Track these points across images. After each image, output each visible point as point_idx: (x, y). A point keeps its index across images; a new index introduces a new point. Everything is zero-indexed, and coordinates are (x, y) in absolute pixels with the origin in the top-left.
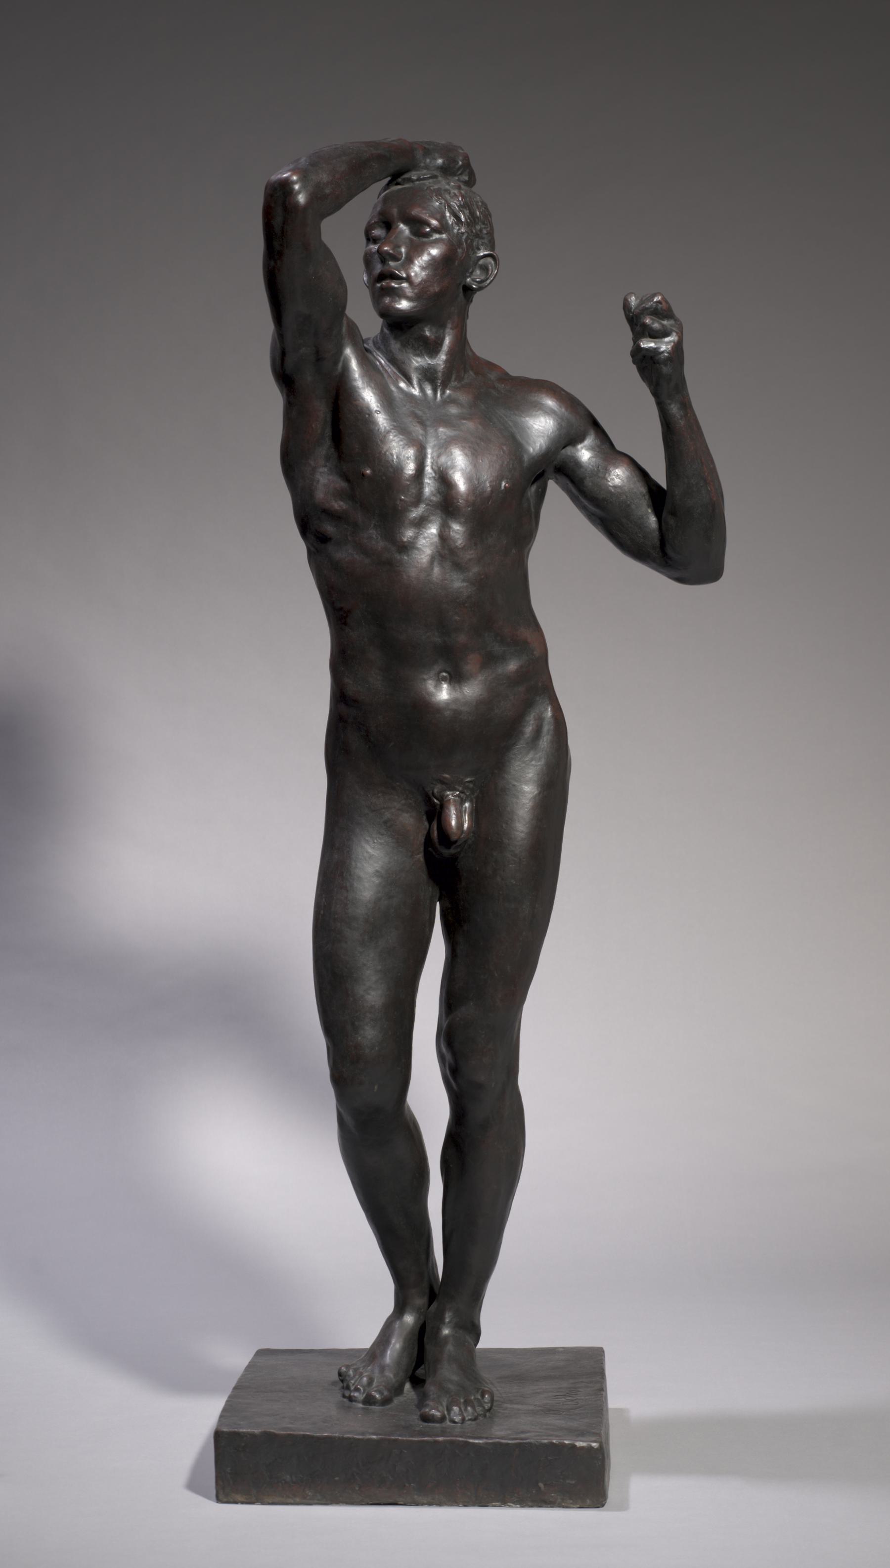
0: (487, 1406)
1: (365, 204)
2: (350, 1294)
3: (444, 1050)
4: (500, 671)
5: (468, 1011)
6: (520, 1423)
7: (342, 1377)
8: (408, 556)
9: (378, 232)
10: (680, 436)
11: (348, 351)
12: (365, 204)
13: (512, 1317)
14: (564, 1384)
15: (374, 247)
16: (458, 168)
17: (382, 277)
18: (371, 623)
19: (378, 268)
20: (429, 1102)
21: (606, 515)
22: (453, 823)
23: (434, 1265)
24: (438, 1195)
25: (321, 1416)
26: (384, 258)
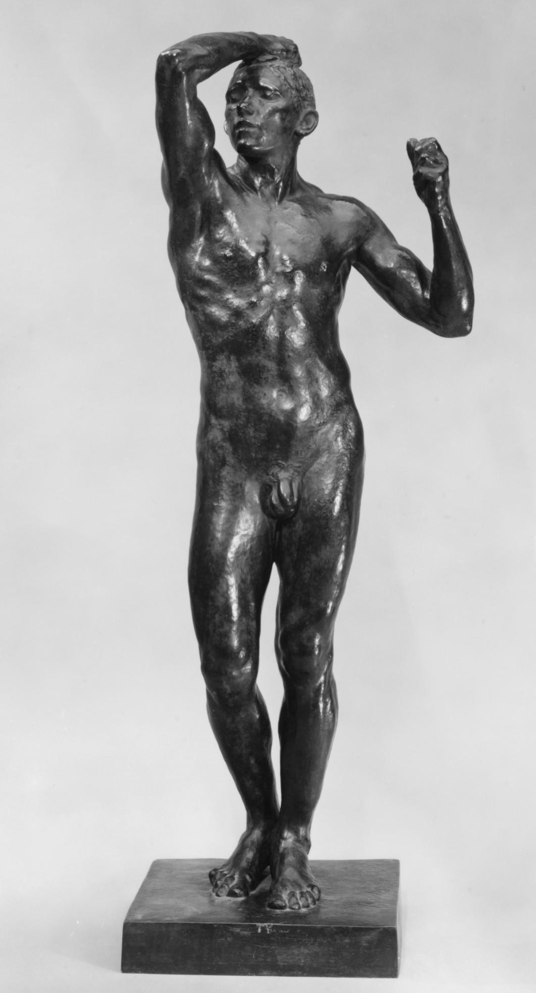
1: (226, 75)
2: (211, 822)
3: (279, 646)
4: (203, 135)
5: (294, 617)
6: (333, 906)
8: (317, 556)
9: (234, 96)
10: (446, 238)
11: (275, 567)
12: (226, 75)
15: (234, 106)
16: (291, 53)
17: (241, 124)
19: (237, 120)
20: (271, 687)
21: (386, 284)
22: (218, 194)
23: (275, 801)
24: (275, 753)
25: (193, 906)
26: (240, 112)
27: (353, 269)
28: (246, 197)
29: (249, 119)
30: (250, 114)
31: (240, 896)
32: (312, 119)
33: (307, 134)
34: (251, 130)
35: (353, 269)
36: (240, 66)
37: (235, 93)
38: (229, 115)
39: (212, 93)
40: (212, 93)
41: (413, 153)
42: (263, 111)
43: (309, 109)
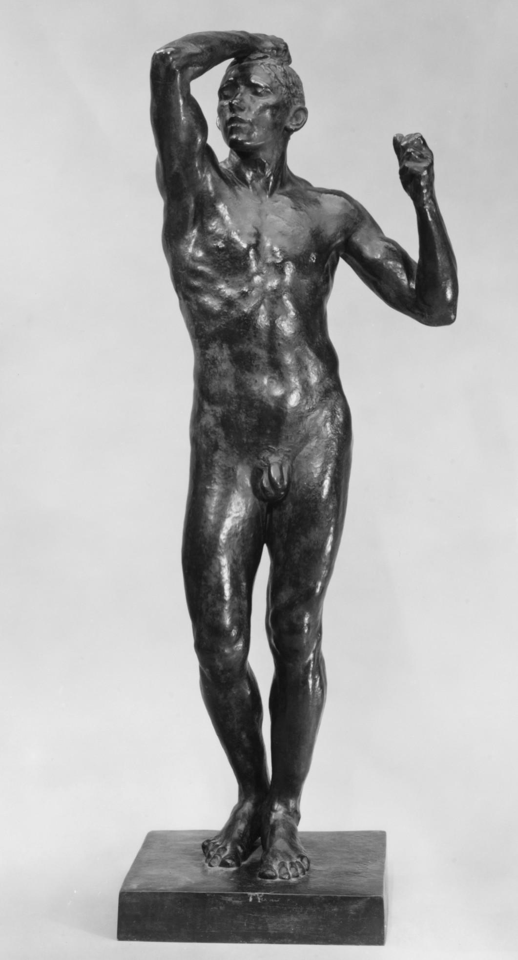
0: (305, 867)
1: (219, 72)
2: (204, 794)
3: (270, 624)
5: (285, 596)
7: (204, 847)
8: (307, 537)
9: (226, 93)
10: (431, 230)
12: (219, 72)
13: (322, 807)
14: (279, 183)
15: (226, 103)
16: (281, 51)
17: (233, 120)
18: (225, 341)
19: (229, 116)
23: (266, 775)
24: (266, 728)
25: (186, 876)
26: (232, 108)
27: (341, 260)
28: (238, 191)
29: (241, 115)
30: (242, 110)
31: (232, 866)
32: (302, 115)
33: (296, 130)
34: (243, 126)
35: (341, 260)
36: (232, 64)
37: (227, 90)
38: (221, 111)
39: (205, 90)
40: (205, 90)
41: (399, 147)
42: (254, 107)
43: (299, 105)
